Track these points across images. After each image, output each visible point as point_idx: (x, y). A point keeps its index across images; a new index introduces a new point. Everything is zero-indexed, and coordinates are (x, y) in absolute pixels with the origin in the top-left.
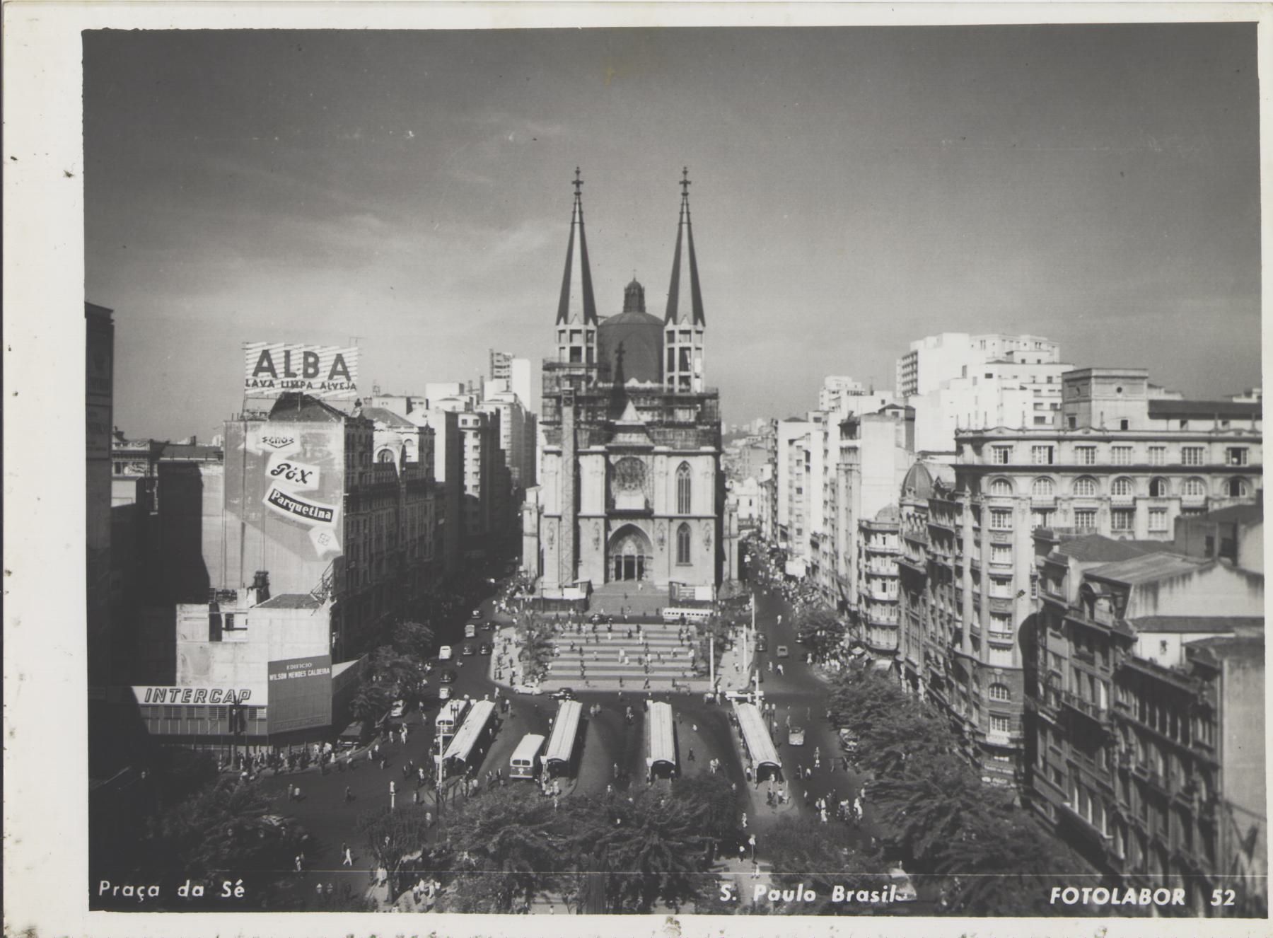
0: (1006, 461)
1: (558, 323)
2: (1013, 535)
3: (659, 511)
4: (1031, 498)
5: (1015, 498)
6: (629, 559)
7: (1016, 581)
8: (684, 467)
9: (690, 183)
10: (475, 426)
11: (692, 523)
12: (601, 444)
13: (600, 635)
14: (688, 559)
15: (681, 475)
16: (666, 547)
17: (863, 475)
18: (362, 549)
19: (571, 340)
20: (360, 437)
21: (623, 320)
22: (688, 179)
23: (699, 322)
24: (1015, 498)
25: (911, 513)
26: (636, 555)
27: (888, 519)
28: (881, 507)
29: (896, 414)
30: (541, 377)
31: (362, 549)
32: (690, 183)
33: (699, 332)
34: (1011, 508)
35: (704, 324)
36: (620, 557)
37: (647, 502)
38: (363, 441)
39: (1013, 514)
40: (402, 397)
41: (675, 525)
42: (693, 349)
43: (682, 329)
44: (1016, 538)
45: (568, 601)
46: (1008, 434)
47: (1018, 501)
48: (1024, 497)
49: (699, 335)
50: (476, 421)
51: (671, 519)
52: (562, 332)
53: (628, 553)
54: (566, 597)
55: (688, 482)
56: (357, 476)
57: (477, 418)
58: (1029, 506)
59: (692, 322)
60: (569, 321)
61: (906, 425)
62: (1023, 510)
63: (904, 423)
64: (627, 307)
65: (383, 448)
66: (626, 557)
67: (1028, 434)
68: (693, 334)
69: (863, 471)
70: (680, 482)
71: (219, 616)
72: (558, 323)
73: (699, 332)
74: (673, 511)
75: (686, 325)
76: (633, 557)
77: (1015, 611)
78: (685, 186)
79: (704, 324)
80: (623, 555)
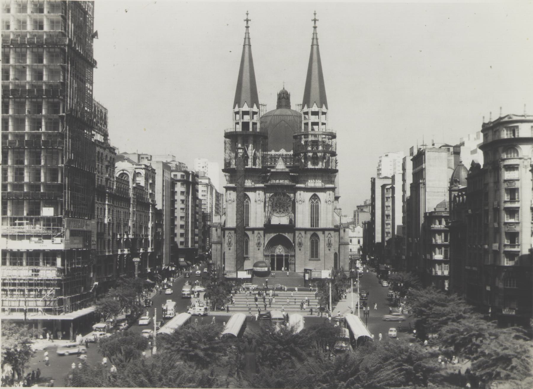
0: (514, 135)
1: (234, 108)
3: (299, 225)
4: (530, 159)
6: (280, 257)
7: (521, 210)
8: (315, 197)
9: (318, 20)
11: (320, 234)
12: (262, 183)
13: (263, 303)
14: (317, 256)
15: (312, 202)
16: (302, 249)
17: (427, 186)
18: (111, 242)
19: (243, 118)
20: (106, 156)
22: (317, 18)
23: (324, 106)
24: (520, 159)
26: (284, 254)
28: (439, 203)
29: (449, 150)
30: (223, 141)
31: (111, 242)
32: (318, 20)
35: (327, 108)
36: (274, 255)
37: (291, 221)
38: (109, 159)
39: (519, 169)
40: (135, 153)
41: (309, 234)
42: (320, 124)
43: (313, 110)
45: (240, 279)
46: (515, 118)
47: (522, 160)
48: (526, 158)
50: (182, 176)
51: (306, 230)
53: (279, 253)
54: (239, 277)
55: (317, 208)
56: (104, 180)
57: (183, 174)
58: (529, 163)
59: (319, 105)
60: (241, 106)
61: (454, 157)
62: (526, 166)
63: (453, 155)
64: (279, 106)
65: (122, 172)
66: (278, 256)
67: (528, 118)
68: (320, 114)
70: (312, 207)
72: (234, 108)
73: (324, 113)
74: (307, 225)
75: (315, 108)
76: (282, 256)
79: (327, 108)
80: (276, 254)
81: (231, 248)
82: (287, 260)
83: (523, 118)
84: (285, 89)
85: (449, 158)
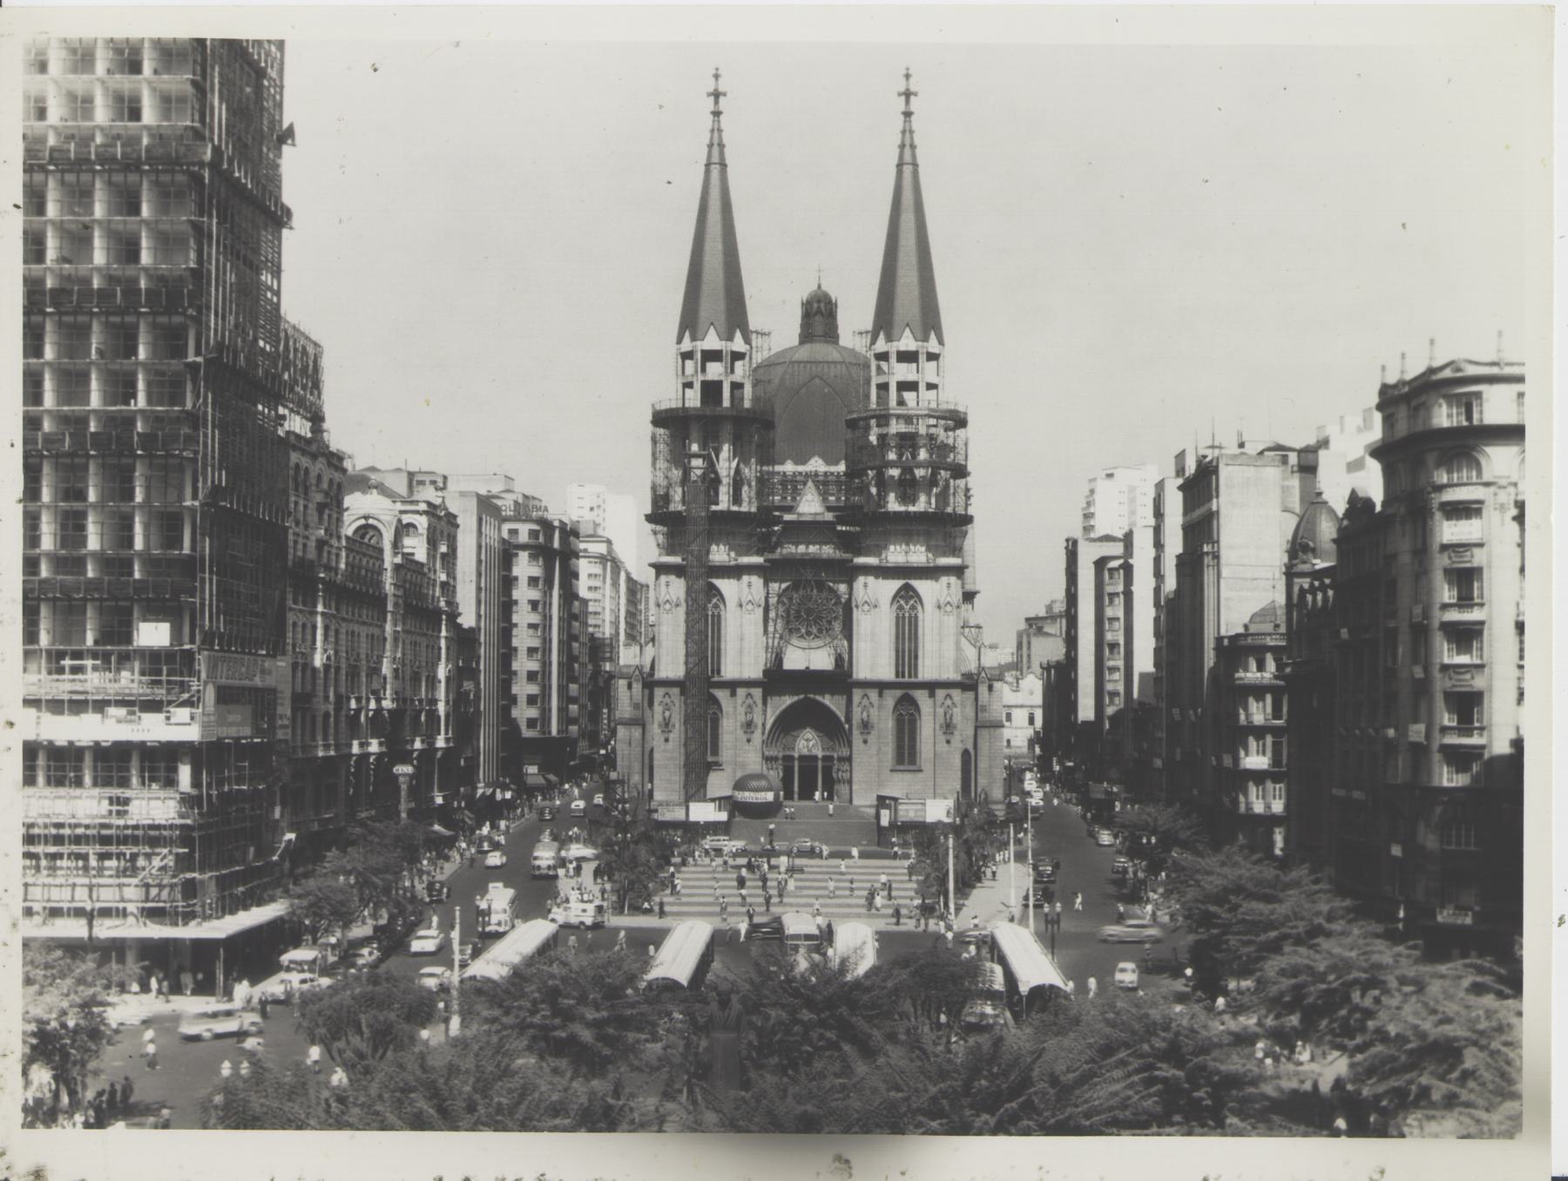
0: (1469, 417)
2: (1485, 548)
3: (862, 672)
4: (1515, 485)
5: (1487, 484)
8: (907, 593)
10: (532, 542)
11: (921, 696)
12: (759, 553)
13: (760, 892)
14: (913, 761)
15: (900, 608)
16: (872, 738)
17: (1223, 561)
19: (704, 370)
21: (797, 357)
24: (1487, 484)
25: (1306, 586)
26: (820, 754)
27: (1268, 628)
29: (1285, 460)
31: (332, 719)
33: (932, 357)
34: (1481, 502)
35: (941, 342)
36: (791, 758)
37: (839, 659)
38: (325, 486)
39: (1485, 513)
40: (399, 470)
41: (891, 698)
42: (922, 387)
43: (902, 348)
44: (1490, 613)
46: (1471, 371)
47: (1492, 489)
48: (1503, 482)
49: (933, 364)
51: (881, 686)
52: (687, 356)
53: (805, 752)
54: (693, 818)
55: (914, 623)
57: (535, 527)
58: (1512, 498)
59: (919, 335)
60: (700, 335)
61: (1301, 480)
63: (1297, 475)
64: (807, 336)
65: (363, 522)
66: (802, 758)
68: (922, 358)
69: (1224, 553)
70: (899, 621)
71: (82, 659)
73: (932, 357)
74: (886, 672)
75: (907, 342)
76: (815, 758)
77: (1490, 690)
78: (907, 102)
79: (941, 342)
81: (671, 736)
82: (827, 771)
83: (1495, 371)
84: (824, 288)
85: (1286, 483)
